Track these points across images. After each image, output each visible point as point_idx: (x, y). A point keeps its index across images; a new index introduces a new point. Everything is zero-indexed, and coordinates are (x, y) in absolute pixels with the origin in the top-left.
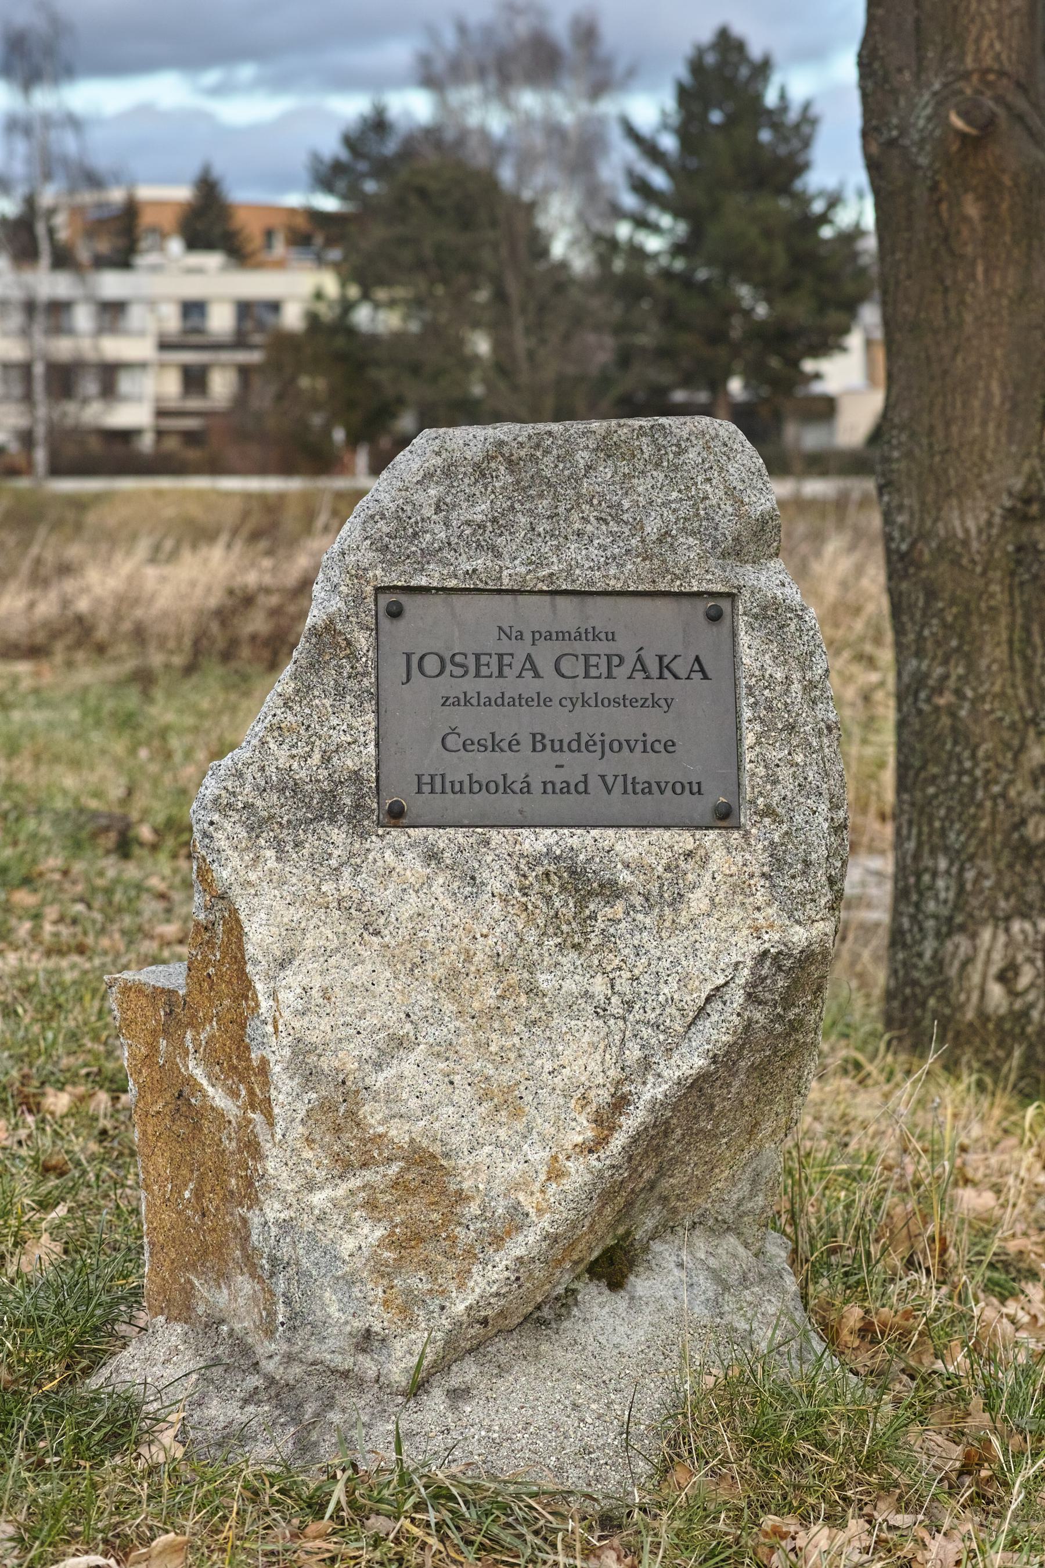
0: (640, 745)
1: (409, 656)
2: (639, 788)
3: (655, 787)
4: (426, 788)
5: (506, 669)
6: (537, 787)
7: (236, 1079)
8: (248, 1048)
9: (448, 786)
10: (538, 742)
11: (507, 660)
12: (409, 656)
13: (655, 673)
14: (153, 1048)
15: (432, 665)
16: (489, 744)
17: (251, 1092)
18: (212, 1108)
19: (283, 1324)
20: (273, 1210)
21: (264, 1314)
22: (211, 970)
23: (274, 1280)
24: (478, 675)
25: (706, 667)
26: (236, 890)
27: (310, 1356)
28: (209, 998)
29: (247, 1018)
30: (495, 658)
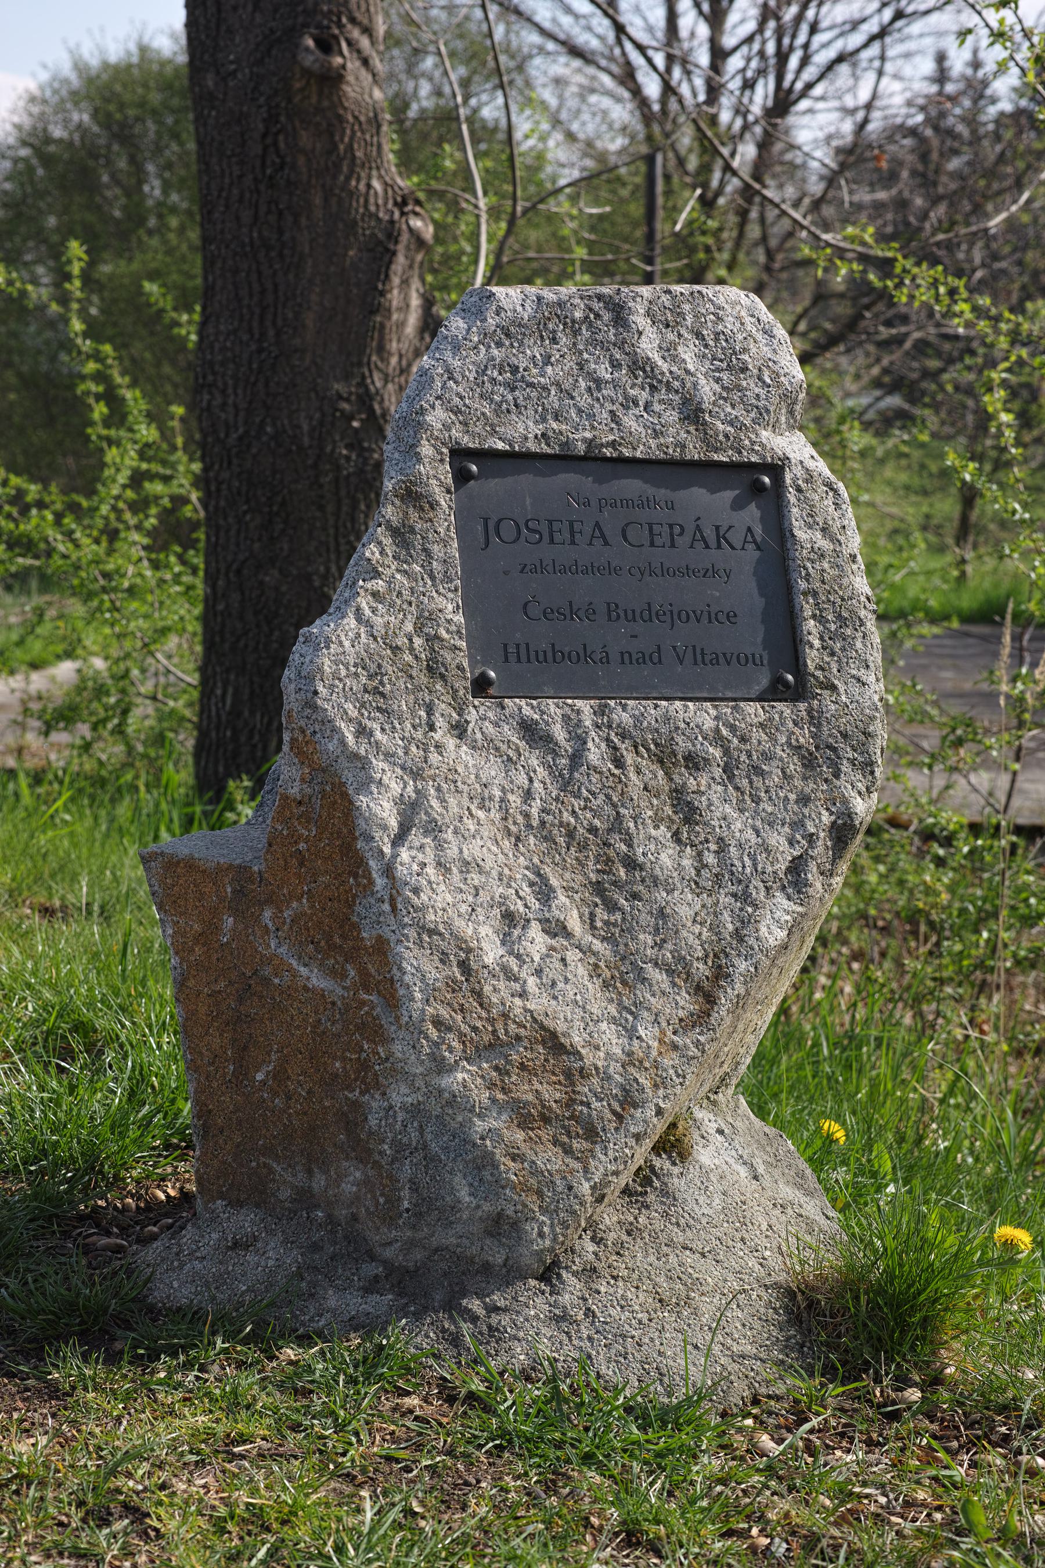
0: (706, 615)
1: (486, 521)
2: (707, 658)
3: (722, 660)
4: (512, 658)
5: (577, 536)
6: (615, 656)
7: (340, 959)
8: (356, 927)
9: (532, 654)
10: (612, 613)
11: (577, 526)
12: (486, 521)
13: (713, 543)
14: (212, 928)
15: (508, 530)
16: (567, 613)
17: (363, 973)
18: (306, 989)
19: (408, 1210)
20: (400, 1095)
21: (381, 1200)
22: (302, 846)
23: (396, 1165)
24: (552, 541)
25: (607, 533)
26: (343, 762)
27: (434, 1242)
28: (298, 875)
29: (355, 896)
30: (666, 528)
